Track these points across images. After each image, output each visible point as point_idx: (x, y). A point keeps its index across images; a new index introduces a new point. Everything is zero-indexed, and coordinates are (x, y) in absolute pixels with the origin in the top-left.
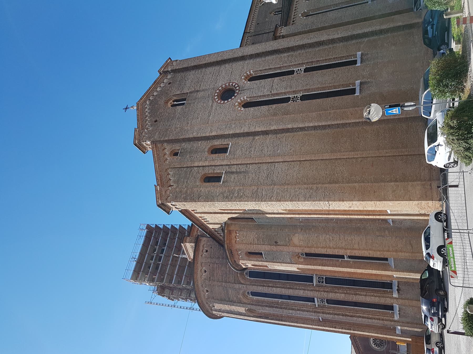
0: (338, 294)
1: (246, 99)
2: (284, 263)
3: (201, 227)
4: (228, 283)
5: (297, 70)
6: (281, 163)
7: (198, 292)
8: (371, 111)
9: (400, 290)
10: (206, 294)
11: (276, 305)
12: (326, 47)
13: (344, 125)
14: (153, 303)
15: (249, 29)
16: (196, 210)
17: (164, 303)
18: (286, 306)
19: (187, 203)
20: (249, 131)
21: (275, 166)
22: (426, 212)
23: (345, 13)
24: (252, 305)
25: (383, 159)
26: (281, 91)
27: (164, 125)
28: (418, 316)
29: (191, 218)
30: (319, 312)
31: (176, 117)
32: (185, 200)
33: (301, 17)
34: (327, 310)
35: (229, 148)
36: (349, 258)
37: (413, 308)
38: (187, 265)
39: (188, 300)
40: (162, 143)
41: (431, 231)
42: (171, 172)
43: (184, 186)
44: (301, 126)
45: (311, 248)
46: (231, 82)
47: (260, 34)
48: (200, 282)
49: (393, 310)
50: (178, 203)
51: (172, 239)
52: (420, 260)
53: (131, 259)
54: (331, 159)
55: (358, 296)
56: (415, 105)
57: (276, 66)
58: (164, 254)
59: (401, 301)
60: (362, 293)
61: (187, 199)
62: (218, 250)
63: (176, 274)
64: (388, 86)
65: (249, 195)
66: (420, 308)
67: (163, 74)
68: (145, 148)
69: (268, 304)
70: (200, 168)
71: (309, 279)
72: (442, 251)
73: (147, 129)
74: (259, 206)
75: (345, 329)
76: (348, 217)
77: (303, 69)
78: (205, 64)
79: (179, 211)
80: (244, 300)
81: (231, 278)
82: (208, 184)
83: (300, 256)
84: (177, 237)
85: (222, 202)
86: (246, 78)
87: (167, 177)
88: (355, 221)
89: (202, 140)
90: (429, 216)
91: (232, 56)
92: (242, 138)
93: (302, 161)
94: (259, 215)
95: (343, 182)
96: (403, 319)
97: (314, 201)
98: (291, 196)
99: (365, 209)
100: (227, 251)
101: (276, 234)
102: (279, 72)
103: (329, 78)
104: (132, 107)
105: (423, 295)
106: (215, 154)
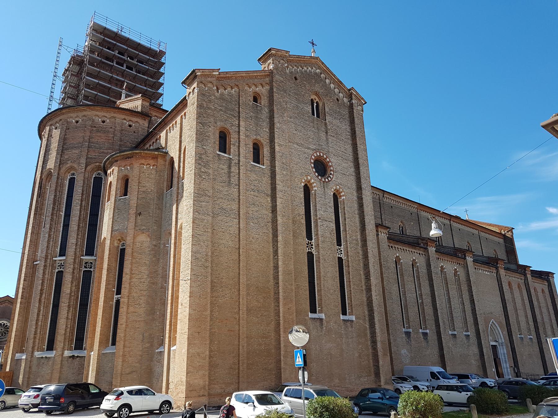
0: (70, 286)
1: (314, 189)
2: (113, 221)
3: (162, 122)
4: (88, 150)
5: (341, 249)
6: (238, 226)
7: (77, 110)
8: (298, 333)
9: (73, 359)
10: (73, 120)
11: (56, 208)
12: (363, 283)
13: (277, 300)
14: (60, 48)
15: (388, 196)
16: (185, 118)
17: (60, 63)
18: (55, 221)
19: (196, 108)
20: (277, 190)
21: (235, 218)
22: (171, 390)
23: (396, 303)
24: (58, 178)
25: (236, 343)
26: (319, 230)
27: (291, 88)
28: (38, 380)
29: (175, 111)
30: (46, 261)
31: (298, 103)
32: (200, 106)
33: (395, 256)
35: (258, 165)
36: (117, 301)
37: (50, 374)
38: (111, 99)
39: (64, 95)
40: (270, 83)
41: (149, 396)
42: (235, 91)
43: (216, 106)
44: (280, 251)
45: (131, 256)
46: (335, 173)
47: (381, 210)
48: (89, 113)
49: (47, 350)
50: (196, 97)
51: (145, 83)
52: (112, 383)
53: (121, 25)
54: (239, 285)
55: (67, 309)
56: (304, 383)
57: (347, 226)
58: (127, 70)
59: (59, 360)
60: (70, 314)
61: (200, 109)
62: (131, 140)
63: (98, 83)
64: (316, 349)
65: (202, 185)
66: (50, 382)
67: (349, 92)
68: (264, 62)
69: (57, 198)
70: (237, 128)
71: (90, 251)
72: (125, 410)
73: (287, 67)
74: (187, 197)
75: (23, 292)
76: (169, 302)
77: (341, 256)
78: (356, 144)
79: (186, 97)
80: (63, 169)
81: (94, 154)
82: (218, 136)
83: (121, 242)
84: (148, 89)
85: (195, 152)
86: (337, 191)
87: (229, 86)
88: (163, 309)
89: (271, 133)
90: (166, 393)
91: (362, 177)
92: (270, 182)
93: (239, 250)
94: (175, 196)
95: (213, 297)
96: (35, 362)
97: (191, 263)
98: (198, 236)
99: (179, 321)
100: (130, 152)
101: (151, 215)
102: (340, 229)
103: (330, 285)
104: (314, 51)
105: (69, 386)
106: (252, 147)
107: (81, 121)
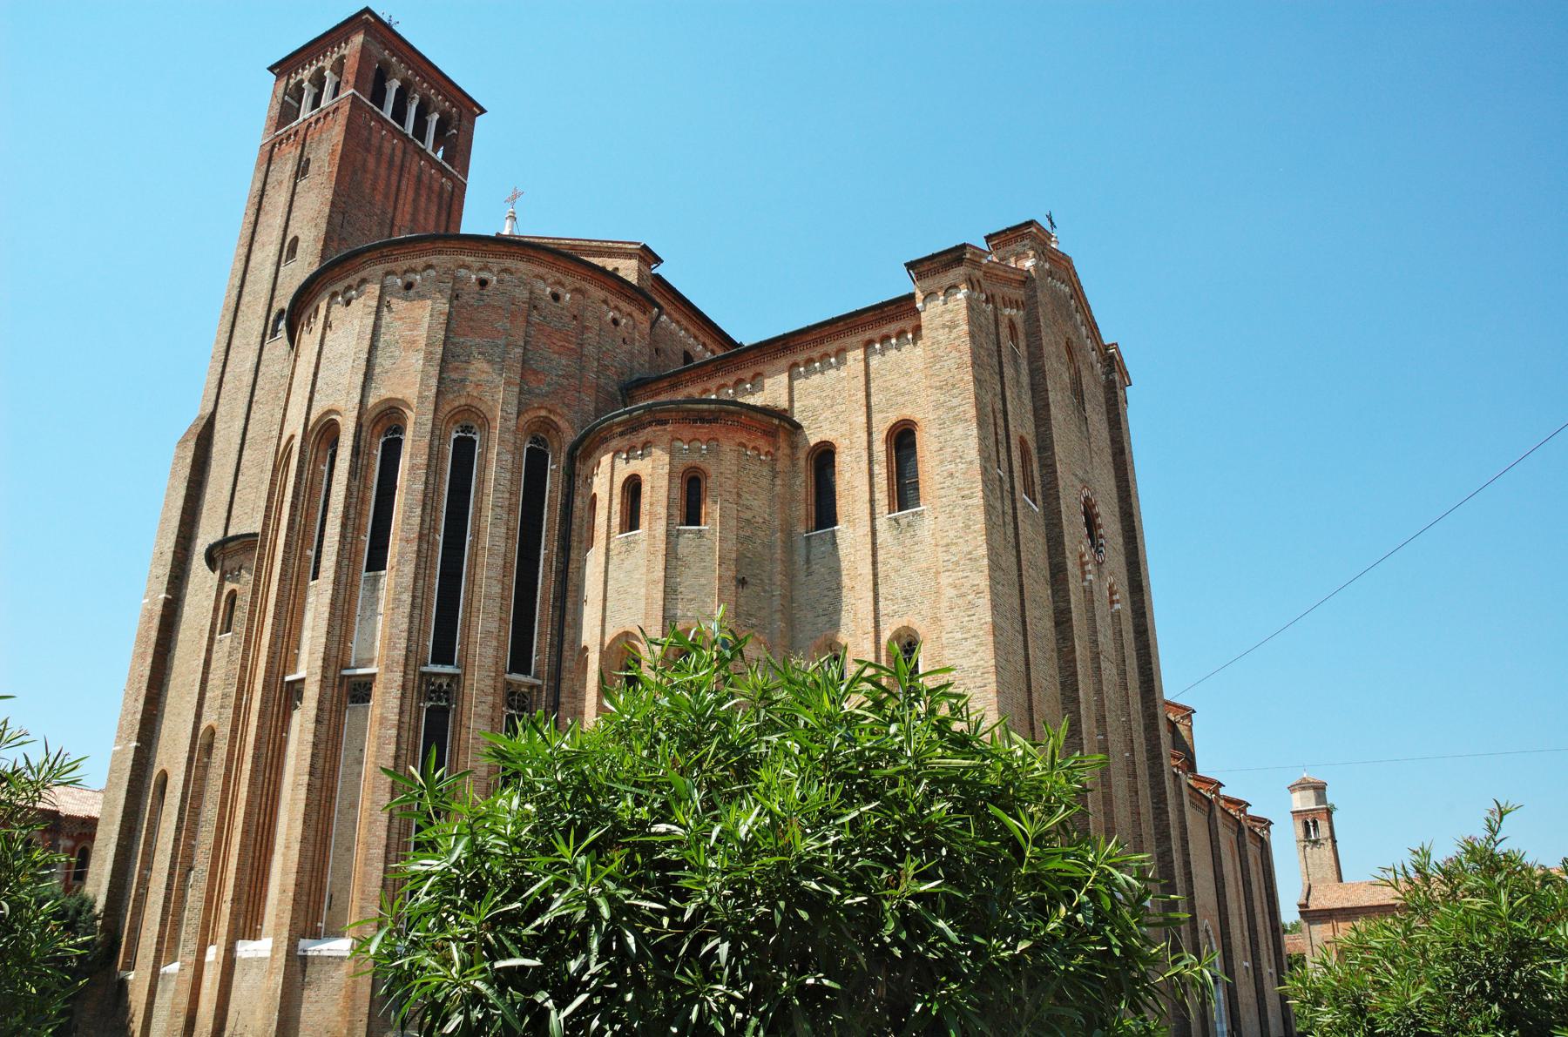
34: (333, 696)
107: (494, 282)
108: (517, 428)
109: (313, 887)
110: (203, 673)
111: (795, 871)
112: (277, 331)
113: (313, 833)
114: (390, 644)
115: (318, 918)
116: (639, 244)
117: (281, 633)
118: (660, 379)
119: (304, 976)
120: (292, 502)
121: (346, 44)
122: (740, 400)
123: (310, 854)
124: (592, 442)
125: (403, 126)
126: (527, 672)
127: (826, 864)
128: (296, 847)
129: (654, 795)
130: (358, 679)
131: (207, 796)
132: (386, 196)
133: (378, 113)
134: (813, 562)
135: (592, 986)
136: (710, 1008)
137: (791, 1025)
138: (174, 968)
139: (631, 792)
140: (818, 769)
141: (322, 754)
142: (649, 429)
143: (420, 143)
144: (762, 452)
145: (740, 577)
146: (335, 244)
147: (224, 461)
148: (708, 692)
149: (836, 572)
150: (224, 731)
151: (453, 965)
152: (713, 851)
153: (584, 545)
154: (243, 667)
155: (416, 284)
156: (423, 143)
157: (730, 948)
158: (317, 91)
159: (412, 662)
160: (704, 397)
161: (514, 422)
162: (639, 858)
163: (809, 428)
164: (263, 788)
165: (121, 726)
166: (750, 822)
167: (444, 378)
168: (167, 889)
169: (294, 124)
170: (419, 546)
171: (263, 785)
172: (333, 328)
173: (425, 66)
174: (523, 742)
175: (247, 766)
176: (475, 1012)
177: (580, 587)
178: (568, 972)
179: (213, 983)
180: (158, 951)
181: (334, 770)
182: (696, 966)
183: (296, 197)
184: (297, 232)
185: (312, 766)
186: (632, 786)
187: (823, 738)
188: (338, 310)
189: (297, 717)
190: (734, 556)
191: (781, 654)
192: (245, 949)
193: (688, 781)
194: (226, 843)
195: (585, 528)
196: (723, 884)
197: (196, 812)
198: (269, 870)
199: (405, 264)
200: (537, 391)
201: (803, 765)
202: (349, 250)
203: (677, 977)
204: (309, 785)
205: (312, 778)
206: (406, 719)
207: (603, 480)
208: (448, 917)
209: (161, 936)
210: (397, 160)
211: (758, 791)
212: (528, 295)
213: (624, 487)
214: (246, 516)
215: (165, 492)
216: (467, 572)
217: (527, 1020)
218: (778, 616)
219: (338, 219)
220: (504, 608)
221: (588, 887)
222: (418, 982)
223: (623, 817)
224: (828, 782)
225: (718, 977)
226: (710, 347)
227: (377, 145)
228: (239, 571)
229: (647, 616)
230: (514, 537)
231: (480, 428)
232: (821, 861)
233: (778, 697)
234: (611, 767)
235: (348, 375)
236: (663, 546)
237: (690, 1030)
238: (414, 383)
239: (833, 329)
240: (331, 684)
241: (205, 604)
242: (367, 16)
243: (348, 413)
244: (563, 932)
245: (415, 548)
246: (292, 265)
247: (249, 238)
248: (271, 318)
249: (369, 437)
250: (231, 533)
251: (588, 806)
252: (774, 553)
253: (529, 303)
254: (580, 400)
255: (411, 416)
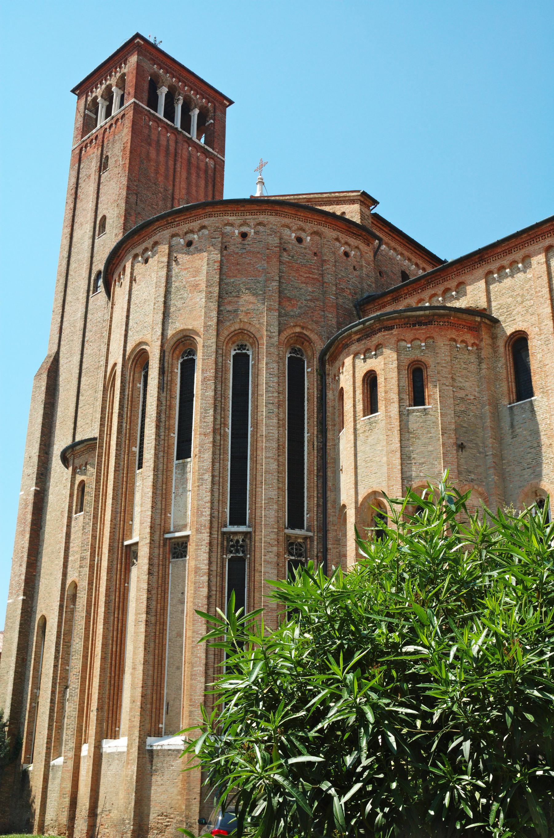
34: (159, 554)
107: (252, 234)
108: (280, 343)
109: (154, 698)
110: (66, 543)
111: (520, 681)
112: (97, 288)
113: (152, 657)
114: (198, 512)
115: (159, 721)
116: (359, 191)
117: (119, 510)
118: (385, 294)
119: (152, 765)
120: (119, 413)
121: (125, 64)
122: (449, 305)
123: (151, 672)
124: (336, 348)
125: (173, 122)
126: (301, 527)
127: (545, 675)
128: (140, 668)
129: (403, 622)
130: (176, 540)
131: (75, 633)
132: (166, 177)
133: (153, 115)
134: (517, 427)
135: (364, 776)
136: (459, 794)
137: (527, 810)
138: (58, 762)
139: (385, 621)
140: (532, 597)
141: (154, 598)
142: (379, 335)
143: (187, 134)
144: (470, 344)
145: (459, 443)
146: (133, 218)
147: (68, 387)
148: (439, 539)
149: (536, 433)
150: (83, 585)
151: (257, 762)
152: (452, 666)
153: (337, 427)
154: (94, 537)
155: (194, 242)
156: (189, 133)
157: (471, 745)
158: (108, 103)
159: (215, 525)
160: (420, 305)
161: (276, 339)
162: (394, 673)
163: (505, 321)
164: (114, 625)
165: (11, 585)
166: (480, 642)
167: (221, 311)
168: (51, 703)
169: (94, 131)
170: (214, 438)
171: (114, 623)
172: (137, 281)
173: (185, 74)
174: (300, 586)
175: (101, 610)
176: (276, 799)
177: (336, 460)
178: (345, 765)
179: (88, 772)
180: (48, 748)
181: (164, 609)
182: (446, 760)
183: (101, 186)
184: (105, 212)
185: (148, 607)
186: (385, 616)
187: (535, 571)
188: (140, 267)
189: (134, 572)
190: (453, 427)
191: (496, 501)
192: (109, 746)
193: (428, 611)
194: (90, 668)
195: (337, 414)
196: (462, 692)
197: (68, 645)
198: (122, 686)
199: (185, 227)
200: (292, 313)
201: (519, 594)
202: (143, 222)
203: (431, 769)
204: (146, 621)
205: (149, 616)
206: (214, 568)
207: (347, 377)
208: (252, 723)
209: (49, 738)
210: (172, 149)
211: (484, 616)
212: (278, 241)
213: (363, 380)
214: (87, 426)
215: (29, 413)
216: (251, 455)
217: (316, 804)
218: (492, 471)
219: (133, 199)
220: (280, 480)
221: (356, 698)
222: (232, 776)
223: (380, 641)
224: (541, 608)
225: (464, 768)
226: (421, 266)
227: (156, 139)
228: (86, 466)
229: (389, 478)
230: (284, 425)
231: (252, 345)
232: (541, 672)
233: (496, 540)
234: (369, 601)
235: (151, 315)
236: (398, 423)
237: (444, 813)
238: (200, 317)
239: (519, 240)
240: (157, 545)
241: (64, 492)
242: (138, 40)
243: (153, 343)
244: (339, 733)
245: (211, 440)
246: (104, 237)
247: (71, 220)
248: (92, 278)
249: (170, 360)
250: (77, 439)
251: (353, 634)
252: (485, 423)
253: (279, 247)
254: (325, 317)
255: (199, 341)
